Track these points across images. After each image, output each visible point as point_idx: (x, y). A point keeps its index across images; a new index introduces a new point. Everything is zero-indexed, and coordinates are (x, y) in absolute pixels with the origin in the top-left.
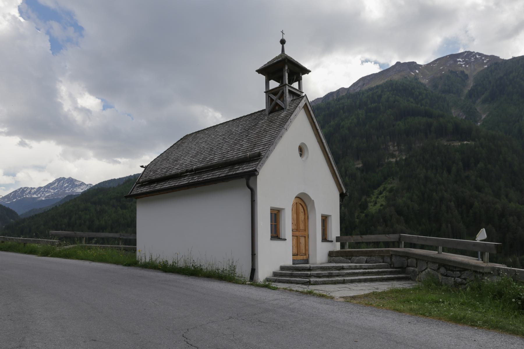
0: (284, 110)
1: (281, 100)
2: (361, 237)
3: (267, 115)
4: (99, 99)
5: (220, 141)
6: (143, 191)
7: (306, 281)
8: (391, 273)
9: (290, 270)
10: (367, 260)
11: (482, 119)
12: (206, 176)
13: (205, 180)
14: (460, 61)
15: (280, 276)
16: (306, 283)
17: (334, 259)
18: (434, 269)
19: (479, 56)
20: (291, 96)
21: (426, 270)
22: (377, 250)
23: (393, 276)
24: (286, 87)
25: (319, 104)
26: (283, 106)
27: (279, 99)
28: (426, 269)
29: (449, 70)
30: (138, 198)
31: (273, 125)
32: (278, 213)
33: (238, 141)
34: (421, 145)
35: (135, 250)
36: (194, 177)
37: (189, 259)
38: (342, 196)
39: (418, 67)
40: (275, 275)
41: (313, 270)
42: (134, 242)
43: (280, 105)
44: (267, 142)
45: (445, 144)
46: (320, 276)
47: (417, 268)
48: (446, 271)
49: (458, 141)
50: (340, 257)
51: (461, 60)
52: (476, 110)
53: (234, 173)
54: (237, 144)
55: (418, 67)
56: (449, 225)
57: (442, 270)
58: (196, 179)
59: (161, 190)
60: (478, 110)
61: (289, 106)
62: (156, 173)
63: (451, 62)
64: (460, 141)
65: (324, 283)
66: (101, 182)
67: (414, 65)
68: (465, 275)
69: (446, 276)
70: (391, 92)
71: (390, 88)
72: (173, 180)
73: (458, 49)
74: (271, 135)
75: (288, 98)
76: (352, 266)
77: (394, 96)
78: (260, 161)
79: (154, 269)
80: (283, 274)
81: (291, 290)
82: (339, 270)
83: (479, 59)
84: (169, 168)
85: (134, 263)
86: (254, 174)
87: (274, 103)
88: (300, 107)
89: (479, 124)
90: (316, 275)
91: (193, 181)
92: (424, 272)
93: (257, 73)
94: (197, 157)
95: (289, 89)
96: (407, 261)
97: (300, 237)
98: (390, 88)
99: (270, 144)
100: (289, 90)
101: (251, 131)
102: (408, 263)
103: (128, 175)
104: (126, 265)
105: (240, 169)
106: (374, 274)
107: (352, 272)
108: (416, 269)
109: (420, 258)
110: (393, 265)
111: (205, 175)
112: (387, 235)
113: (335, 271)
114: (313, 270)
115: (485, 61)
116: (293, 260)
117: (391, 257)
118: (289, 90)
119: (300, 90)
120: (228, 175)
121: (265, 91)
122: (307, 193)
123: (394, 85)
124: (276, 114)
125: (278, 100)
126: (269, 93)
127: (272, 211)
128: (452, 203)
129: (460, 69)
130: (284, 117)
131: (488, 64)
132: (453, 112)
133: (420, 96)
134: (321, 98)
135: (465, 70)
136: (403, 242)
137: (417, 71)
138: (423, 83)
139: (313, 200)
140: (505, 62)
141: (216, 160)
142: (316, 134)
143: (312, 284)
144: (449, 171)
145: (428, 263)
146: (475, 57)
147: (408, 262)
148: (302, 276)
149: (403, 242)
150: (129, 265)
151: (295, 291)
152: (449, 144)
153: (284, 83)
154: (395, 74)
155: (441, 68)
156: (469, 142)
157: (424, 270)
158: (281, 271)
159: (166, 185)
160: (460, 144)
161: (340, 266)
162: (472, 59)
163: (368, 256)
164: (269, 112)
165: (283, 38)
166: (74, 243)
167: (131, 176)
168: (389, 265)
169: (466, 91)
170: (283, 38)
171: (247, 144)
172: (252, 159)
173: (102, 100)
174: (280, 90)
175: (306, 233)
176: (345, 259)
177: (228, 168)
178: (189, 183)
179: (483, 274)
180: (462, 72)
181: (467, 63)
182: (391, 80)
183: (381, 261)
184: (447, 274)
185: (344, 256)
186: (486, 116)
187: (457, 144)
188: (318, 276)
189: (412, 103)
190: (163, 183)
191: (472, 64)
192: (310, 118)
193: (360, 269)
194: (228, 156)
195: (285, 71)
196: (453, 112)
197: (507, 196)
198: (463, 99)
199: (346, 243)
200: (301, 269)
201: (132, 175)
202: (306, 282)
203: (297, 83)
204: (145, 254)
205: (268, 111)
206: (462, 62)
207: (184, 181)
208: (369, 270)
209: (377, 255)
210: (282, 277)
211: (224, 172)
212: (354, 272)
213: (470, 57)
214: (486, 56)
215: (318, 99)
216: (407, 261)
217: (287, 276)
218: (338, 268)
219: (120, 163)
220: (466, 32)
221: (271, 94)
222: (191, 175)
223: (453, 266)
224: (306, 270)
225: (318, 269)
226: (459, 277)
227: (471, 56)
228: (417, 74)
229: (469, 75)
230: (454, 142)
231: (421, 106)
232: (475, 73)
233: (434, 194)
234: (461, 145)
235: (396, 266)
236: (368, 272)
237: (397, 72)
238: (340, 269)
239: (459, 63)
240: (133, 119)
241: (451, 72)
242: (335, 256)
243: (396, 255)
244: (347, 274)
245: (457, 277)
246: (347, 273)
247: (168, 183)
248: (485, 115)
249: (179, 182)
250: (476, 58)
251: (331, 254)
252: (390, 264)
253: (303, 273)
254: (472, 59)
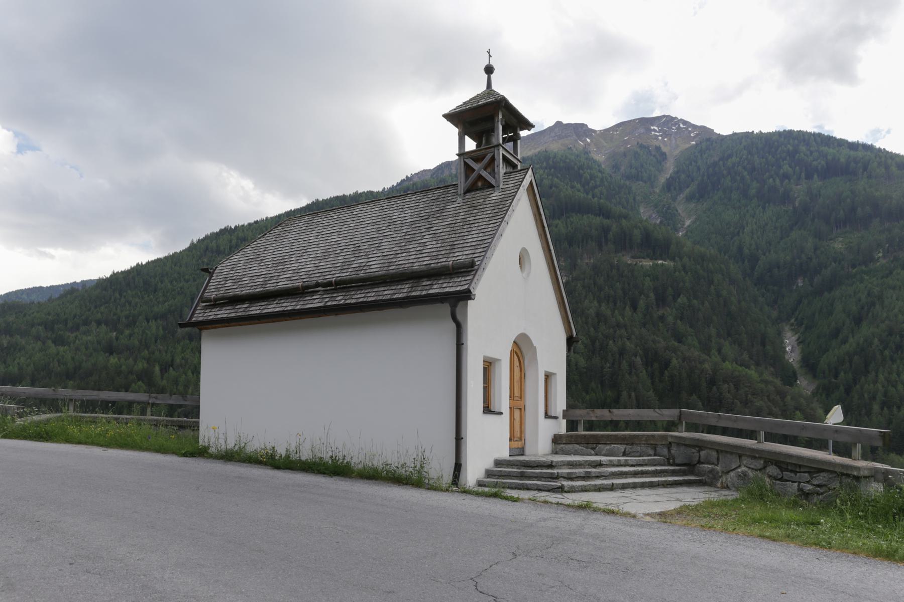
0: (496, 188)
1: (489, 170)
2: (610, 411)
3: (460, 195)
4: (8, 130)
5: (369, 234)
6: (219, 316)
7: (557, 485)
8: (673, 473)
9: (514, 467)
10: (627, 450)
11: (685, 226)
12: (363, 295)
13: (362, 302)
14: (655, 130)
15: (498, 476)
16: (556, 489)
17: (564, 448)
18: (756, 468)
19: (683, 125)
21: (739, 470)
22: (643, 435)
23: (681, 478)
24: (499, 150)
25: (427, 181)
26: (493, 182)
27: (485, 169)
28: (739, 466)
29: (638, 144)
30: (206, 329)
31: (480, 214)
32: (489, 366)
33: (412, 236)
34: (592, 261)
35: (196, 427)
36: (335, 295)
37: (325, 445)
38: (571, 341)
39: (590, 133)
40: (488, 475)
41: (556, 466)
42: (195, 411)
44: (478, 243)
45: (629, 262)
46: (572, 477)
47: (719, 465)
48: (780, 473)
49: (648, 259)
50: (575, 445)
51: (656, 128)
52: (677, 211)
53: (424, 293)
54: (411, 241)
55: (590, 133)
56: (633, 394)
57: (773, 470)
58: (340, 299)
59: (274, 315)
60: (680, 211)
61: (504, 182)
62: (239, 283)
63: (642, 131)
64: (651, 259)
65: (584, 489)
66: (11, 291)
67: (584, 129)
68: (821, 479)
69: (781, 479)
70: (546, 171)
71: (545, 164)
72: (287, 299)
73: (652, 111)
74: (482, 231)
75: (502, 169)
76: (613, 460)
77: (550, 177)
78: (475, 275)
79: (248, 463)
80: (506, 474)
81: (546, 502)
82: (595, 467)
83: (684, 129)
84: (270, 275)
85: (202, 453)
86: (467, 295)
87: (473, 176)
89: (680, 233)
90: (566, 476)
91: (334, 303)
92: (732, 474)
93: (445, 120)
94: (328, 260)
95: (504, 153)
96: (698, 454)
97: (514, 409)
98: (545, 164)
99: (486, 246)
101: (435, 220)
102: (700, 458)
103: (69, 280)
104: (185, 455)
105: (435, 286)
106: (649, 475)
107: (619, 471)
108: (717, 467)
109: (722, 450)
110: (674, 459)
111: (358, 293)
112: (657, 410)
113: (590, 468)
114: (556, 468)
115: (692, 135)
116: (511, 449)
117: (669, 446)
120: (410, 296)
121: (458, 153)
122: (528, 334)
123: (551, 159)
124: (478, 194)
125: (483, 170)
126: (466, 157)
127: (486, 363)
128: (638, 359)
129: (655, 143)
130: (499, 200)
131: (697, 139)
132: (642, 211)
133: (592, 182)
134: (430, 170)
135: (662, 146)
136: (684, 422)
137: (588, 140)
138: (597, 160)
139: (535, 347)
140: (722, 138)
141: (375, 267)
142: (541, 235)
143: (566, 492)
144: (634, 307)
145: (743, 458)
146: (677, 126)
147: (700, 455)
148: (543, 477)
149: (684, 422)
150: (192, 455)
151: (555, 503)
152: (634, 263)
154: (553, 140)
155: (626, 138)
156: (665, 261)
157: (734, 469)
158: (496, 467)
159: (273, 307)
160: (651, 263)
161: (597, 461)
162: (673, 129)
163: (627, 444)
164: (465, 190)
165: (489, 62)
166: (58, 410)
167: (75, 283)
168: (666, 460)
169: (662, 180)
170: (489, 62)
171: (434, 243)
172: (455, 271)
173: (16, 135)
174: (487, 154)
175: (522, 402)
176: (584, 448)
177: (406, 284)
178: (325, 307)
179: (857, 478)
180: (658, 148)
181: (665, 134)
182: (547, 150)
183: (652, 452)
184: (782, 477)
185: (581, 443)
186: (691, 221)
187: (647, 263)
188: (570, 478)
189: (579, 191)
190: (263, 304)
191: (672, 136)
192: (535, 206)
193: (625, 466)
194: (400, 263)
195: (498, 121)
196: (642, 211)
197: (719, 351)
198: (658, 191)
199: (580, 420)
200: (536, 465)
201: (78, 281)
202: (557, 487)
204: (225, 434)
205: (462, 189)
206: (658, 132)
207: (315, 302)
208: (640, 469)
209: (643, 442)
210: (504, 479)
211: (402, 291)
212: (622, 472)
213: (670, 125)
214: (695, 127)
215: (425, 171)
216: (698, 454)
217: (513, 478)
218: (593, 465)
219: (52, 257)
220: (666, 84)
222: (326, 292)
223: (795, 464)
224: (543, 466)
225: (564, 465)
226: (808, 482)
227: (672, 124)
228: (589, 144)
229: (667, 154)
230: (643, 260)
231: (593, 198)
232: (677, 152)
233: (611, 342)
234: (653, 265)
235: (678, 461)
236: (642, 471)
237: (556, 138)
238: (597, 466)
239: (653, 133)
240: (81, 176)
241: (641, 146)
242: (564, 444)
243: (678, 444)
244: (612, 475)
245: (804, 483)
246: (612, 472)
247: (277, 303)
248: (690, 221)
249: (301, 303)
250: (679, 128)
251: (557, 440)
252: (667, 459)
253: (545, 473)
254: (673, 129)
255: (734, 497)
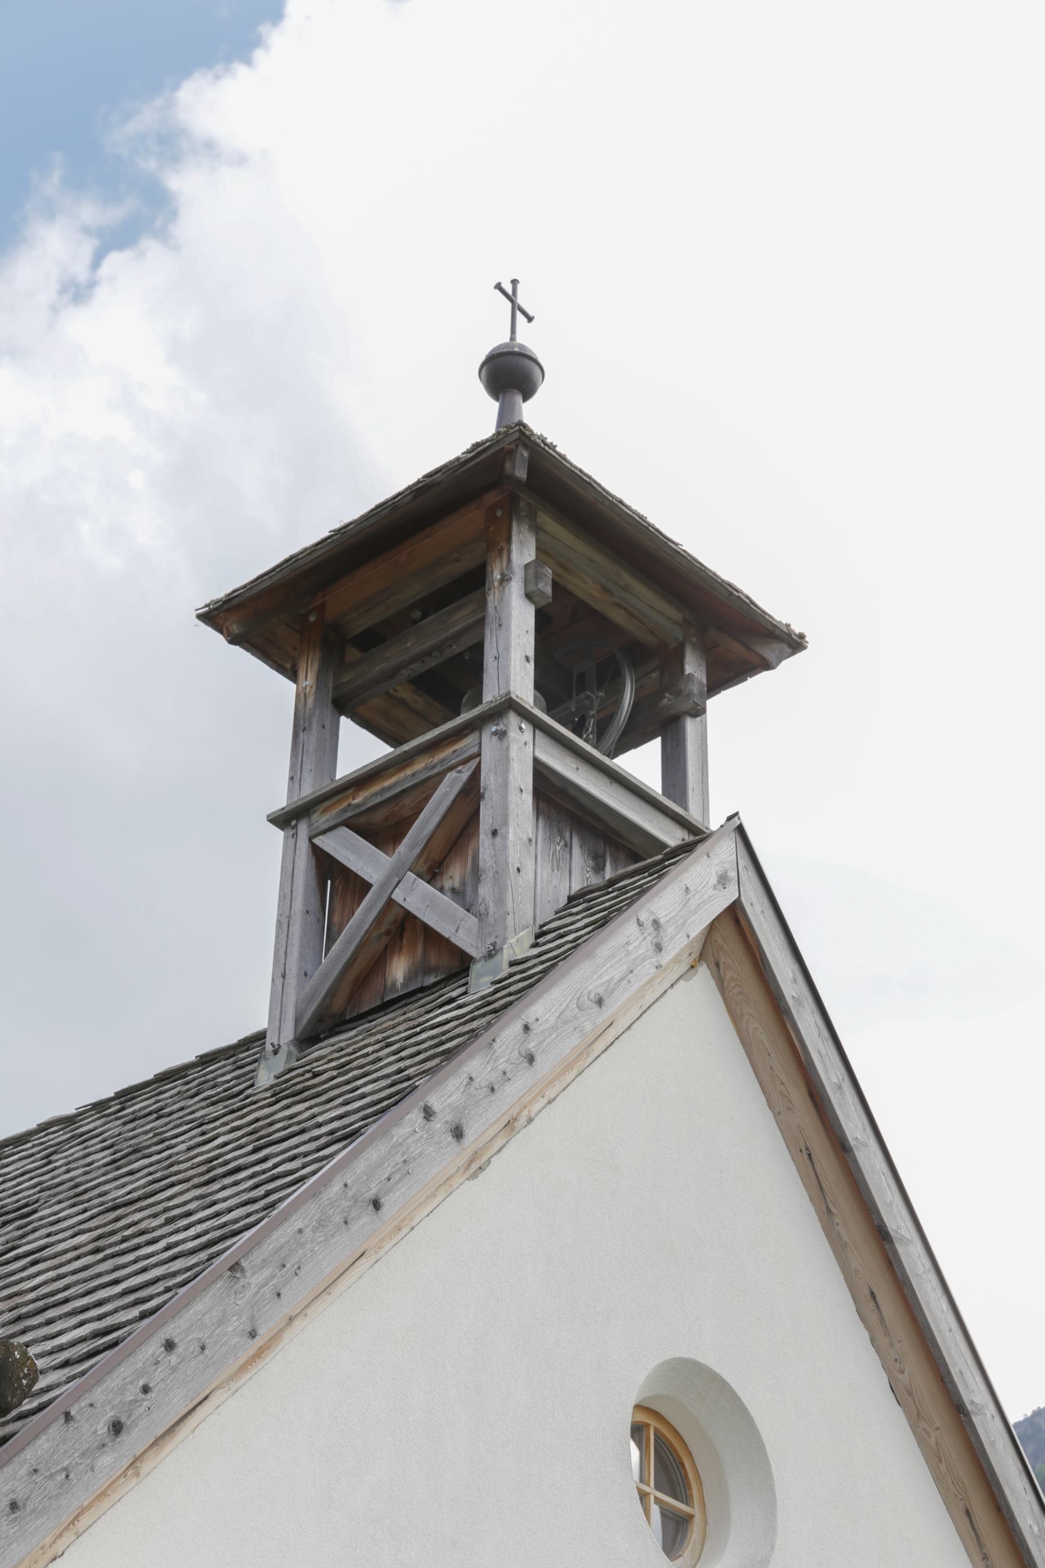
1: (455, 875)
20: (568, 846)
24: (502, 735)
43: (431, 936)
88: (656, 923)
100: (542, 775)
118: (656, 1498)
119: (683, 803)
121: (280, 800)
125: (411, 876)
126: (321, 820)
153: (490, 694)
165: (513, 339)
170: (513, 339)
174: (441, 775)
192: (798, 1095)
195: (505, 579)
203: (654, 746)
221: (344, 831)
255: (197, 1349)
